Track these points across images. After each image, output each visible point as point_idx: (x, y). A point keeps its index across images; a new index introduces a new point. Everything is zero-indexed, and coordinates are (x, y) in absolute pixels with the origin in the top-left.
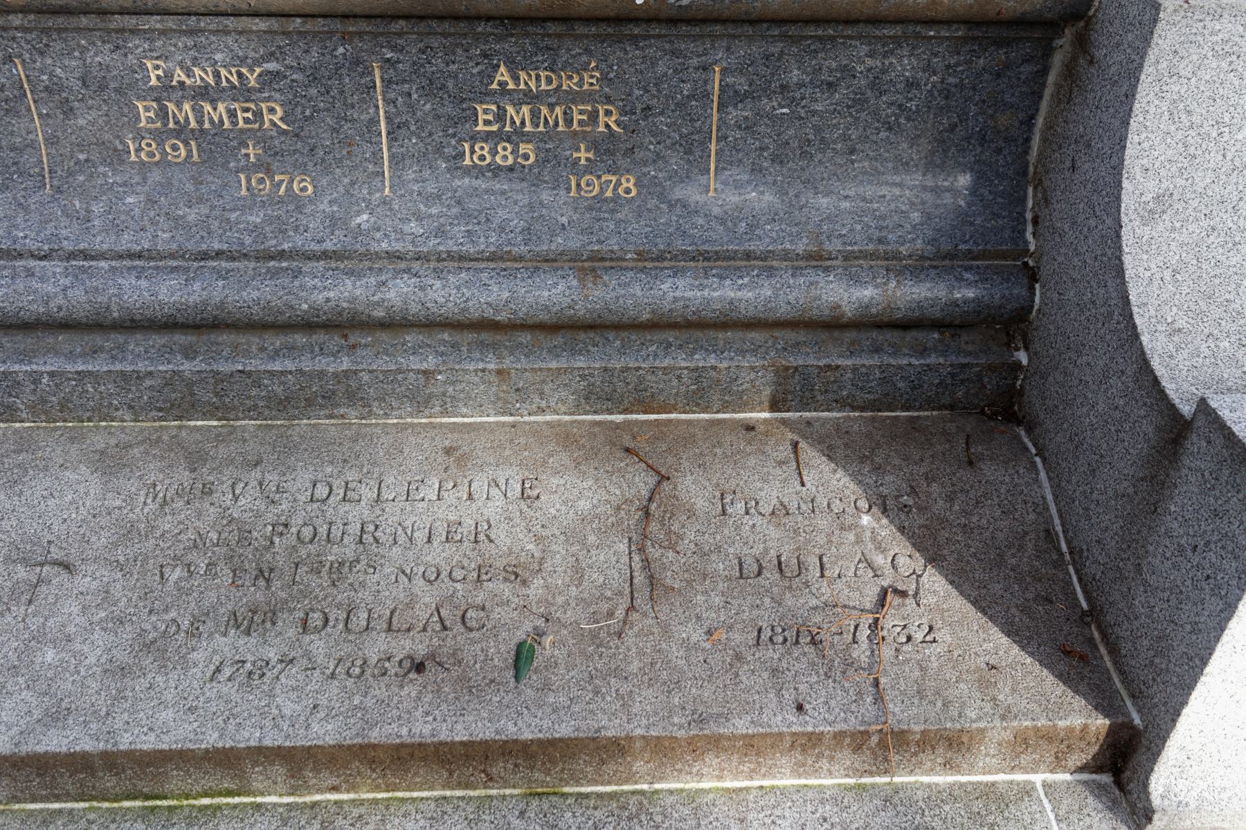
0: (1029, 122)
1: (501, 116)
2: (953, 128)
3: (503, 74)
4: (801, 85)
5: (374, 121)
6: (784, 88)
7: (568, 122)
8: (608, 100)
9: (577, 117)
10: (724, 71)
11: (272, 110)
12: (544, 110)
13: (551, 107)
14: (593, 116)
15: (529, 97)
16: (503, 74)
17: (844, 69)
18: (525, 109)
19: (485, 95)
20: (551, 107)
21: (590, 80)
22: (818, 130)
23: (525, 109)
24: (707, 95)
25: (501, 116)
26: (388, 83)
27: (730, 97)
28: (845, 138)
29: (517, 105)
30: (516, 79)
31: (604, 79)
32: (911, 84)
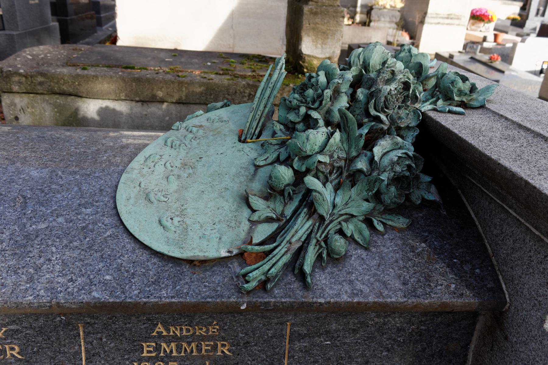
0: (466, 347)
1: (158, 348)
2: (424, 350)
3: (160, 328)
4: (337, 331)
5: (79, 353)
6: (327, 332)
7: (199, 350)
8: (224, 339)
9: (204, 348)
10: (292, 325)
11: (12, 349)
12: (185, 345)
13: (189, 344)
14: (215, 348)
15: (175, 338)
16: (160, 328)
17: (362, 323)
18: (173, 345)
19: (148, 338)
20: (189, 344)
21: (213, 330)
22: (347, 352)
23: (173, 345)
24: (283, 336)
25: (158, 348)
26: (87, 334)
27: (295, 337)
28: (362, 355)
29: (168, 343)
30: (168, 331)
31: (221, 329)
32: (399, 330)
